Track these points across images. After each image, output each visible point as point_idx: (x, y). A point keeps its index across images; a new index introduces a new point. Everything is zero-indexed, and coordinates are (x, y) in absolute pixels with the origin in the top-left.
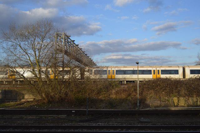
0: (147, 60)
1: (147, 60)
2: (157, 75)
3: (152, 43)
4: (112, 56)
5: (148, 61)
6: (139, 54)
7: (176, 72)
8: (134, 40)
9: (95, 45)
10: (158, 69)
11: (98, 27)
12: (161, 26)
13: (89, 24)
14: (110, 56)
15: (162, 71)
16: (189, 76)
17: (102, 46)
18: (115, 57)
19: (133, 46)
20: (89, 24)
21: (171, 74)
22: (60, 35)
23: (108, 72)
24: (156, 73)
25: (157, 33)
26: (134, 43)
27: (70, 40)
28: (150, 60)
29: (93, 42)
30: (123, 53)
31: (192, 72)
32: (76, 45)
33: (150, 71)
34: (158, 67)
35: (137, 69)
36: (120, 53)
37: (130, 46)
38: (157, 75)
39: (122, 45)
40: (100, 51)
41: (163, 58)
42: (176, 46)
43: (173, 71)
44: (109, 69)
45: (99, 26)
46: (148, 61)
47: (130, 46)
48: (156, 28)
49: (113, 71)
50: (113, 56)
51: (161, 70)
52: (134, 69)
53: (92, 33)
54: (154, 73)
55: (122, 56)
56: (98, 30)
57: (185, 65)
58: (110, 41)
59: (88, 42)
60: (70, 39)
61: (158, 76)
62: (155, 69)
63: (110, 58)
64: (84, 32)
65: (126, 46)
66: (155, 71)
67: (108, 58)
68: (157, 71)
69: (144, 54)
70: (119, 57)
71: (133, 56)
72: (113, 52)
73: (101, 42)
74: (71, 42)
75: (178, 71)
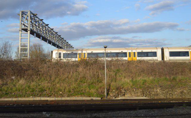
0: (139, 43)
1: (139, 43)
2: (133, 57)
3: (145, 23)
4: (98, 39)
5: (139, 44)
6: (129, 36)
7: (154, 54)
8: (125, 20)
9: (79, 27)
10: (134, 51)
11: (85, 6)
12: (157, 5)
13: (74, 3)
14: (97, 39)
15: (138, 53)
16: (167, 57)
17: (87, 28)
18: (101, 41)
19: (124, 27)
20: (74, 3)
21: (148, 57)
22: (25, 13)
23: (128, 55)
24: (131, 56)
25: (152, 12)
26: (125, 24)
27: (38, 19)
28: (142, 43)
29: (78, 23)
30: (111, 36)
31: (172, 54)
32: (45, 24)
33: (126, 53)
34: (134, 49)
35: (104, 52)
36: (107, 36)
37: (119, 27)
38: (133, 57)
39: (111, 26)
40: (82, 33)
41: (157, 41)
42: (172, 27)
43: (152, 54)
44: (84, 52)
45: (85, 5)
46: (139, 44)
47: (119, 27)
48: (151, 6)
49: (84, 54)
50: (100, 39)
51: (138, 52)
52: (108, 52)
53: (77, 13)
54: (130, 56)
55: (110, 38)
56: (84, 10)
57: (164, 47)
58: (98, 22)
59: (73, 24)
60: (37, 18)
61: (134, 58)
62: (130, 51)
63: (96, 41)
64: (68, 12)
65: (115, 28)
66: (131, 53)
67: (94, 41)
68: (133, 54)
69: (135, 37)
70: (107, 40)
71: (123, 39)
72: (99, 34)
73: (87, 23)
74: (39, 21)
75: (155, 53)
